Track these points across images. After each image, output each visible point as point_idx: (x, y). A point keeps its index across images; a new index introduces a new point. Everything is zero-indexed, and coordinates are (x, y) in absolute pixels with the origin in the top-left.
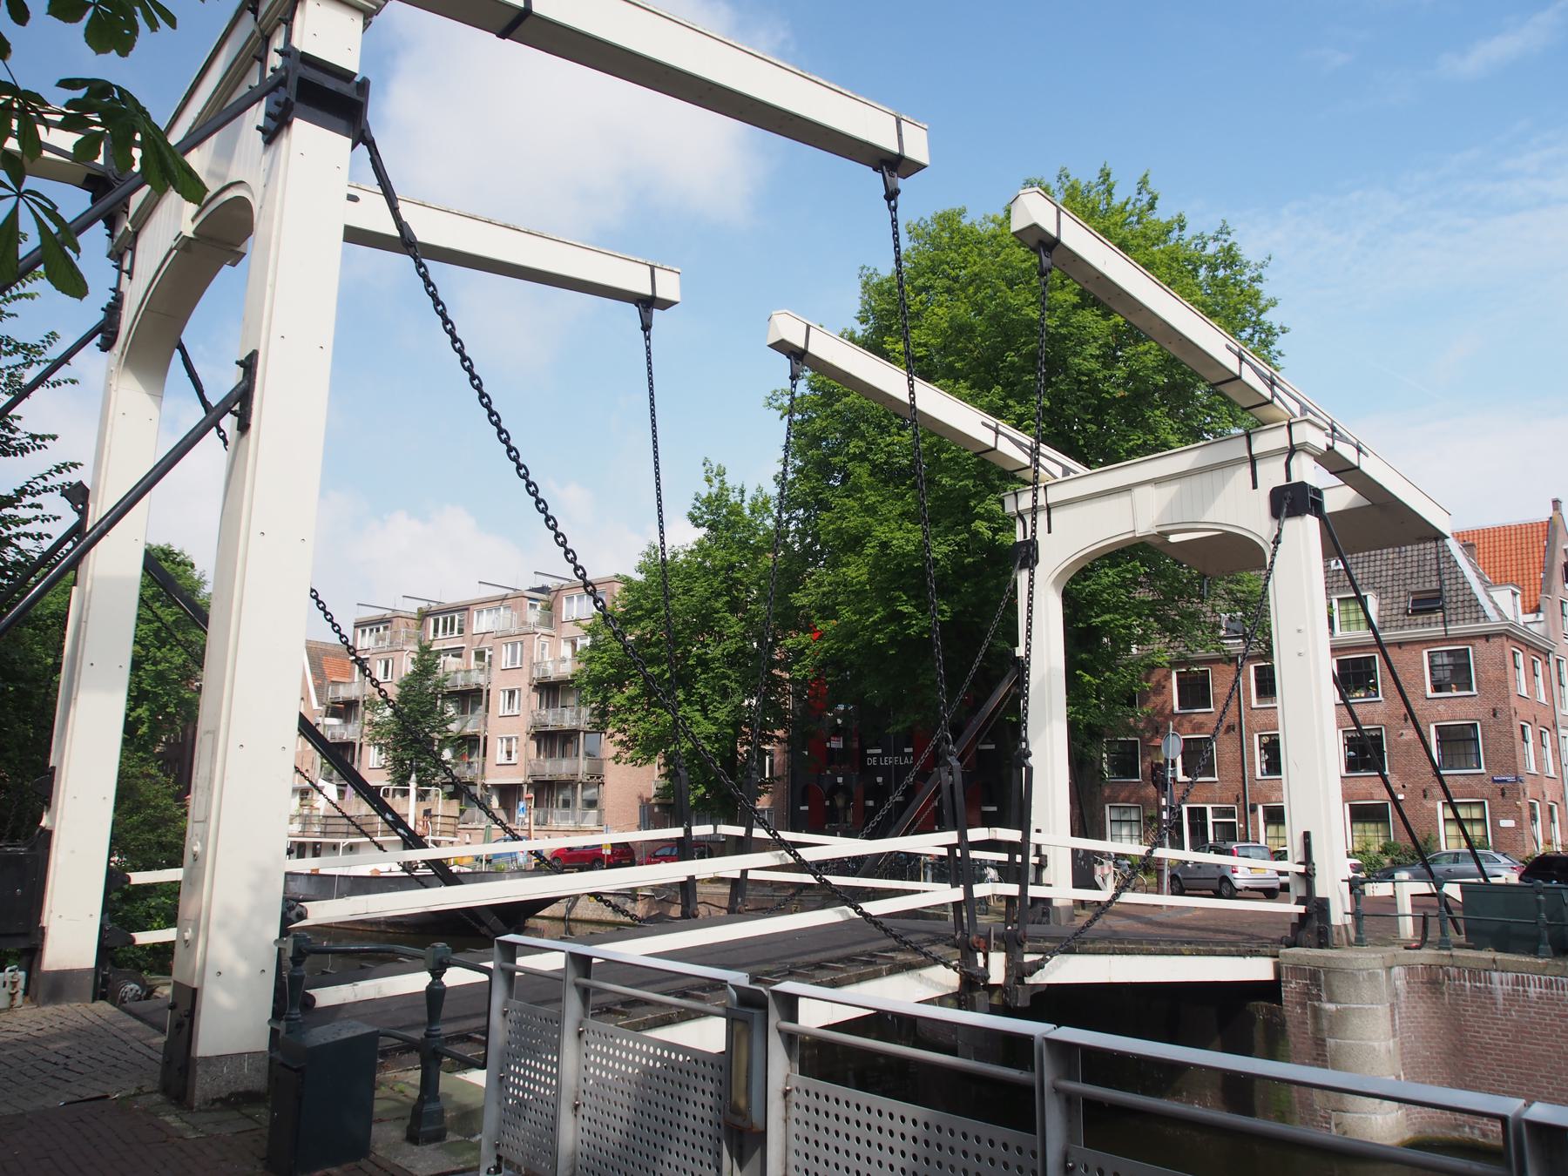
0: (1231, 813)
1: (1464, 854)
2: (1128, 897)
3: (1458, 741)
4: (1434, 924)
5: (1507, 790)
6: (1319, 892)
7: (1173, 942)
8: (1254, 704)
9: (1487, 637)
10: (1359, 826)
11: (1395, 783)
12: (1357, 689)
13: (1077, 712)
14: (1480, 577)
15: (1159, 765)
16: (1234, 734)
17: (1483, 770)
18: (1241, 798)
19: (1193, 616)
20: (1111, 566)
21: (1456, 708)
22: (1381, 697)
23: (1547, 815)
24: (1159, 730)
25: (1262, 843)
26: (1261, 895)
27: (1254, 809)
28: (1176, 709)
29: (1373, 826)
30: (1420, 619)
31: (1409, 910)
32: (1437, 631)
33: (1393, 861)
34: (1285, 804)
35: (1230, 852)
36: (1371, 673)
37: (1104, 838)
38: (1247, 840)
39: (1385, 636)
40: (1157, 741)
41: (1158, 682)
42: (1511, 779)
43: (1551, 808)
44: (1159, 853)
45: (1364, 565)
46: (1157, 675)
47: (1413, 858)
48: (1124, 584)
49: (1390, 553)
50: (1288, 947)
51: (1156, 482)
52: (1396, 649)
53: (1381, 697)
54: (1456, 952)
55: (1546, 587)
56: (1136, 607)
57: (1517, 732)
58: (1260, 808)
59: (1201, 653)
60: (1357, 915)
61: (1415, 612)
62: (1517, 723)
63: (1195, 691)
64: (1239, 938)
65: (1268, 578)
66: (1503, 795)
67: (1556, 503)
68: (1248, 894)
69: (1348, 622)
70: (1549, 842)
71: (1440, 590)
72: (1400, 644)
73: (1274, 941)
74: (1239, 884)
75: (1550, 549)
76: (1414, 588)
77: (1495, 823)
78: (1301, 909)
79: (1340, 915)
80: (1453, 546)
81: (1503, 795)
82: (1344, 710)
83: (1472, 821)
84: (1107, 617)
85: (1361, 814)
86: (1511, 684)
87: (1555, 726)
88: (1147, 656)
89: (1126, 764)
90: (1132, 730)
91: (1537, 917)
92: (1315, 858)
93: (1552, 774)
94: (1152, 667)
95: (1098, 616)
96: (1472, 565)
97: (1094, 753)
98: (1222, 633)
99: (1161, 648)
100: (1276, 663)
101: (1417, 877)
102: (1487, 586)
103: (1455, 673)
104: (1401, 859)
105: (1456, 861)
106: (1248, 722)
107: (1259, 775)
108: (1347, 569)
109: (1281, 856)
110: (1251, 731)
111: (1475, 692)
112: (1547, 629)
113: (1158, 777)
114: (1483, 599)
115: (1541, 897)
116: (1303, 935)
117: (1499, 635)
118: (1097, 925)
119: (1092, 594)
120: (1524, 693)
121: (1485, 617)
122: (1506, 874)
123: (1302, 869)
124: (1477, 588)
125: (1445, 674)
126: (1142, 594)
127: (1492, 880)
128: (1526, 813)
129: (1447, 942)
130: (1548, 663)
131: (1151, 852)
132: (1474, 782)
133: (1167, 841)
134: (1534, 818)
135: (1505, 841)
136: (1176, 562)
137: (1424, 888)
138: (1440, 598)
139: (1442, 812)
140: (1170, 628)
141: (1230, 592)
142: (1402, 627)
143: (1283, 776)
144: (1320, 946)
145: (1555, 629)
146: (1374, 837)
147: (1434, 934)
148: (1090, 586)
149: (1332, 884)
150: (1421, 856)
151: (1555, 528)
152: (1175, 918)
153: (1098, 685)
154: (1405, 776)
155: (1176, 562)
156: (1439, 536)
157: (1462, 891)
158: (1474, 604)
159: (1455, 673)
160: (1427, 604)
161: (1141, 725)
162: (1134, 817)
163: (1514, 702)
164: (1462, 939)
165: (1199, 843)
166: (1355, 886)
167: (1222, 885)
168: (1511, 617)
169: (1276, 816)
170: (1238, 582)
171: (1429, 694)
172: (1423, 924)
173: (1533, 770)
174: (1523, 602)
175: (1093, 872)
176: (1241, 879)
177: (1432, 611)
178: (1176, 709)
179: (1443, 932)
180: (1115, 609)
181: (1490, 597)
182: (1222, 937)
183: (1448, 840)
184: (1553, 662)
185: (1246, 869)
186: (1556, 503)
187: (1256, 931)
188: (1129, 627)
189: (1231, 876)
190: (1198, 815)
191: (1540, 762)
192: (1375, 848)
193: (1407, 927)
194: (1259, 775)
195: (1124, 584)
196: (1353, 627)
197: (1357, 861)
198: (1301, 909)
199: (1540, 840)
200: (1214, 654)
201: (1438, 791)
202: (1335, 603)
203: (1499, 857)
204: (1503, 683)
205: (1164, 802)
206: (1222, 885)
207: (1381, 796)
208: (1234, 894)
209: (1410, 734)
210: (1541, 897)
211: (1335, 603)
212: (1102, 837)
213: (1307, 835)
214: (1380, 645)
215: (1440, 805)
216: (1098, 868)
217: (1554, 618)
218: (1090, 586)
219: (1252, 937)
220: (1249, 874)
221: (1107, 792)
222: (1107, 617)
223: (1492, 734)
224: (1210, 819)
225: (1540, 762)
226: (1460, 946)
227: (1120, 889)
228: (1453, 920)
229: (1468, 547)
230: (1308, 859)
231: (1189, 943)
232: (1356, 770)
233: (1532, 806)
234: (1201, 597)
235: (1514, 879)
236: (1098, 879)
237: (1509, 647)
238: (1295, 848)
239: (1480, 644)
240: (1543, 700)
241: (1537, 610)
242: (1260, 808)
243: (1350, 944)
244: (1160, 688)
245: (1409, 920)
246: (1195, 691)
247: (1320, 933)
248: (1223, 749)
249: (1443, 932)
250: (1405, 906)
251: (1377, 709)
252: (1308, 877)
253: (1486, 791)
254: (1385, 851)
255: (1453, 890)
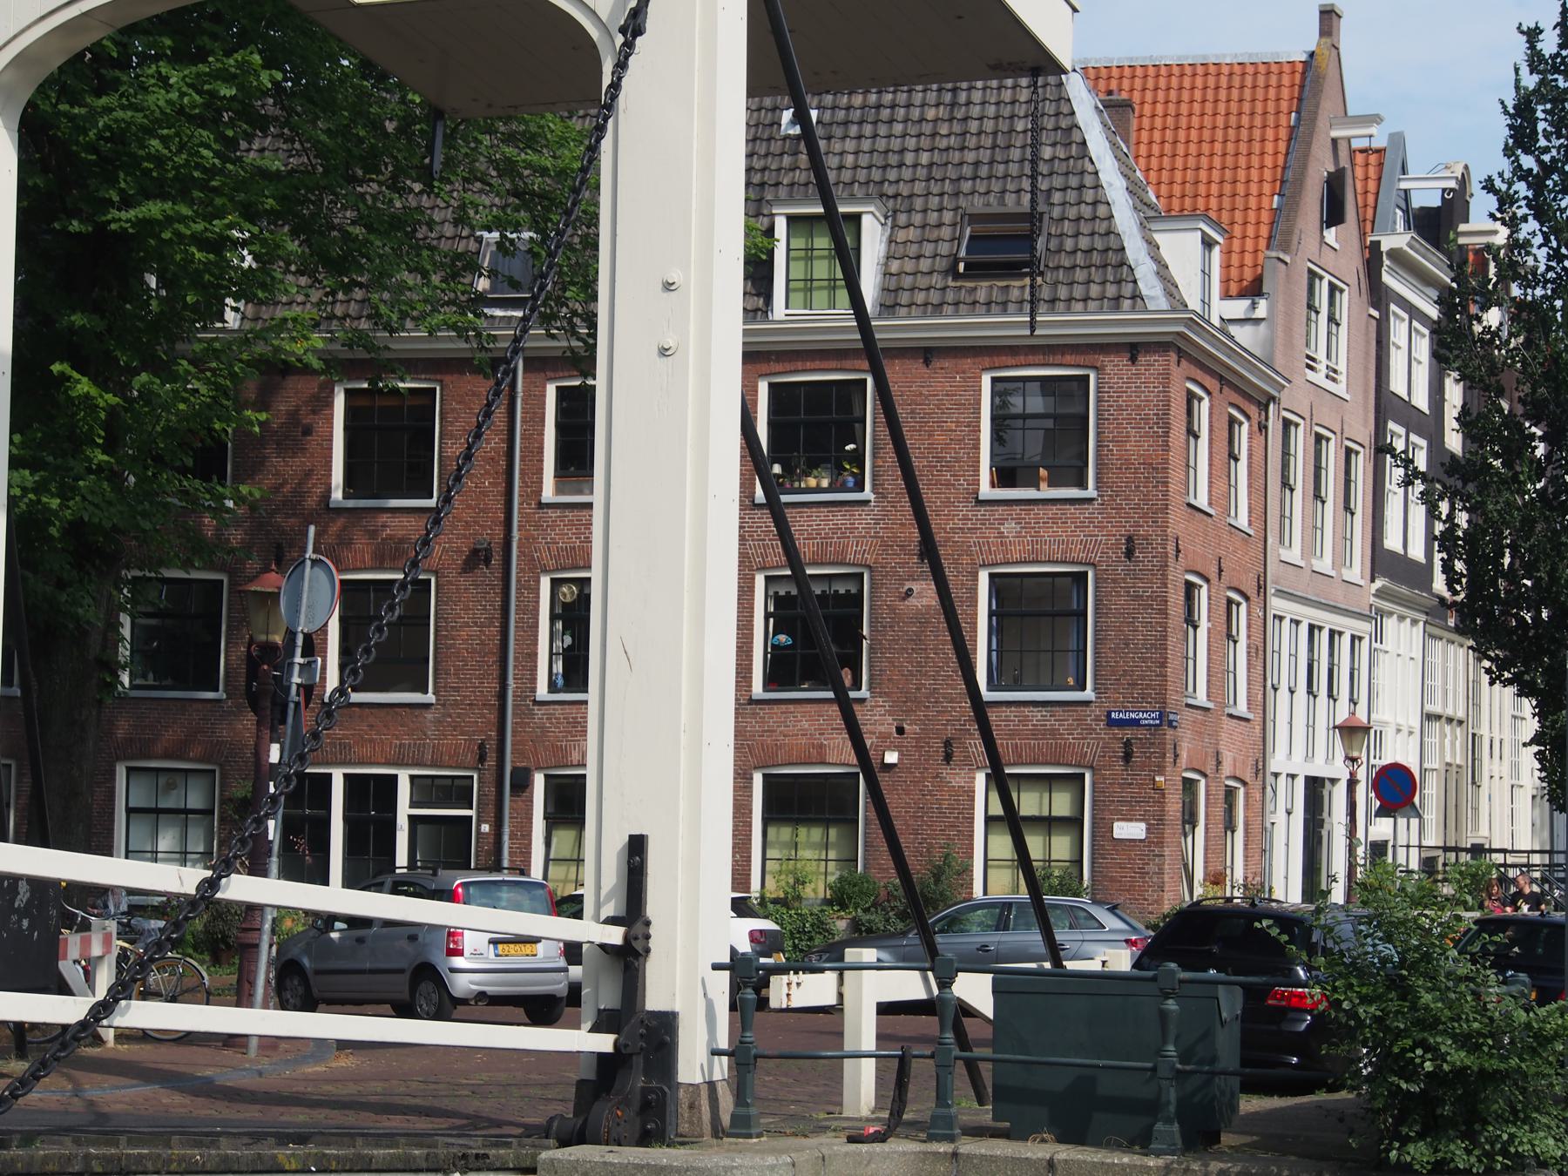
0: (458, 792)
1: (1021, 905)
2: (141, 1014)
3: (1039, 617)
4: (923, 1071)
5: (1139, 741)
6: (655, 1000)
7: (257, 1137)
8: (548, 493)
9: (1134, 349)
10: (784, 833)
11: (876, 720)
12: (812, 466)
13: (40, 488)
14: (1134, 190)
15: (269, 649)
16: (489, 575)
17: (1089, 694)
18: (489, 753)
19: (401, 226)
20: (179, 57)
21: (1043, 530)
22: (868, 493)
23: (1219, 810)
24: (283, 555)
25: (536, 873)
26: (520, 1012)
27: (522, 784)
28: (337, 495)
29: (816, 833)
30: (983, 289)
31: (868, 1042)
32: (1009, 324)
33: (856, 925)
34: (591, 773)
35: (449, 895)
36: (851, 428)
37: (106, 849)
38: (498, 868)
39: (887, 329)
40: (271, 581)
41: (293, 415)
42: (1147, 718)
43: (1230, 793)
44: (240, 888)
45: (855, 126)
46: (293, 393)
47: (902, 916)
48: (209, 116)
49: (926, 101)
50: (564, 1143)
51: (1232, 338)
52: (917, 366)
53: (868, 493)
54: (968, 1146)
55: (1280, 233)
56: (241, 185)
57: (1176, 598)
58: (539, 781)
59: (413, 338)
60: (742, 1057)
61: (977, 270)
62: (1178, 575)
63: (393, 447)
64: (442, 1123)
65: (600, 130)
66: (1127, 757)
67: (1328, 16)
68: (482, 1009)
69: (809, 285)
70: (1216, 879)
71: (1033, 217)
72: (927, 353)
73: (530, 1131)
74: (462, 985)
75: (1299, 137)
76: (977, 205)
77: (1102, 829)
78: (604, 1043)
79: (698, 1058)
80: (1079, 92)
81: (1127, 757)
82: (766, 520)
83: (1048, 824)
84: (154, 209)
85: (793, 801)
86: (1176, 476)
87: (1262, 587)
88: (260, 336)
89: (181, 650)
90: (198, 549)
91: (1159, 1052)
92: (652, 909)
93: (1242, 708)
94: (278, 370)
95: (127, 203)
96: (1120, 157)
97: (89, 612)
98: (483, 284)
99: (305, 315)
100: (600, 383)
101: (905, 962)
102: (1149, 217)
103: (1047, 440)
104: (876, 919)
105: (1002, 925)
106: (527, 540)
107: (542, 691)
108: (808, 134)
109: (570, 906)
110: (535, 569)
111: (1091, 492)
112: (1270, 343)
113: (265, 693)
114: (1135, 250)
115: (1171, 1005)
116: (606, 1113)
117: (1161, 346)
118: (35, 1097)
119: (119, 136)
120: (1202, 501)
121: (1136, 296)
122: (1111, 955)
123: (615, 935)
124: (1125, 218)
125: (1031, 445)
126: (266, 153)
127: (1070, 965)
128: (1174, 805)
129: (949, 1121)
130: (1263, 428)
131: (211, 884)
132: (1063, 723)
133: (274, 863)
134: (1190, 819)
135: (1120, 873)
136: (366, 67)
137: (910, 986)
138: (1029, 239)
139: (982, 799)
140: (334, 262)
141: (508, 168)
142: (938, 308)
143: (592, 695)
144: (645, 1139)
145: (1289, 344)
146: (816, 861)
147: (919, 1107)
148: (111, 111)
149: (688, 978)
150: (915, 912)
151: (1319, 81)
152: (280, 1076)
153: (112, 411)
154: (906, 703)
155: (366, 67)
156: (1039, 64)
157: (997, 991)
158: (1114, 261)
159: (1047, 440)
160: (1003, 251)
161: (236, 537)
162: (195, 800)
163: (1177, 521)
164: (986, 1115)
165: (369, 868)
166: (748, 979)
167: (417, 981)
168: (1194, 303)
169: (568, 804)
170: (531, 141)
171: (986, 490)
172: (897, 1081)
173: (1201, 698)
174: (1226, 266)
175: (53, 951)
176: (469, 970)
177: (1011, 269)
178: (337, 495)
179: (942, 1097)
180: (180, 188)
181: (1153, 246)
182: (395, 1123)
183: (989, 871)
184: (1274, 426)
185: (479, 933)
186: (1328, 16)
187: (487, 1107)
188: (220, 245)
189: (442, 963)
190: (372, 798)
191: (1220, 675)
192: (816, 891)
193: (863, 1085)
194: (542, 691)
195: (209, 116)
196: (820, 297)
197: (768, 925)
198: (604, 1043)
199: (1199, 875)
200: (448, 343)
201: (976, 745)
202: (781, 226)
203: (1101, 914)
204: (1157, 471)
205: (274, 753)
206: (417, 981)
207: (839, 758)
208: (447, 1007)
209: (925, 595)
210: (1171, 1005)
211: (781, 226)
212: (103, 847)
213: (637, 845)
214: (871, 351)
215: (980, 779)
216: (72, 942)
217: (1289, 315)
218: (111, 111)
219: (475, 1122)
220: (490, 959)
221: (122, 728)
222: (154, 209)
223: (1119, 602)
224: (404, 809)
225: (1220, 675)
226: (978, 1132)
227: (122, 990)
228: (971, 1066)
229: (1116, 109)
230: (633, 912)
231: (302, 1139)
232: (790, 684)
233: (1189, 785)
234: (426, 175)
235: (1122, 960)
236: (70, 970)
237: (1182, 380)
238: (602, 877)
239: (1116, 366)
240: (1242, 521)
241: (1254, 290)
242: (539, 781)
243: (718, 1132)
244: (301, 433)
245: (868, 1067)
246: (393, 447)
247: (646, 1106)
248: (455, 616)
249: (942, 1097)
250: (863, 1031)
251: (848, 523)
252: (628, 959)
253: (1091, 748)
254: (839, 898)
255: (975, 990)
